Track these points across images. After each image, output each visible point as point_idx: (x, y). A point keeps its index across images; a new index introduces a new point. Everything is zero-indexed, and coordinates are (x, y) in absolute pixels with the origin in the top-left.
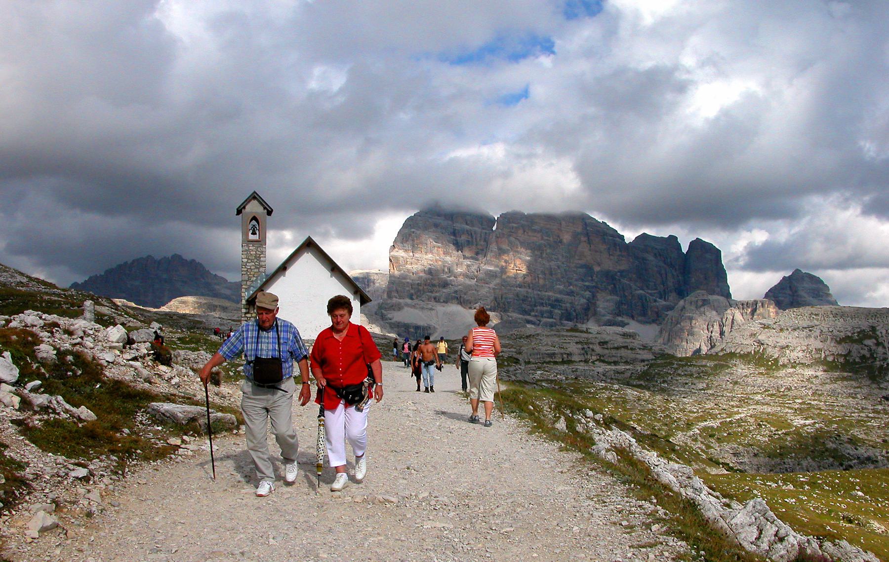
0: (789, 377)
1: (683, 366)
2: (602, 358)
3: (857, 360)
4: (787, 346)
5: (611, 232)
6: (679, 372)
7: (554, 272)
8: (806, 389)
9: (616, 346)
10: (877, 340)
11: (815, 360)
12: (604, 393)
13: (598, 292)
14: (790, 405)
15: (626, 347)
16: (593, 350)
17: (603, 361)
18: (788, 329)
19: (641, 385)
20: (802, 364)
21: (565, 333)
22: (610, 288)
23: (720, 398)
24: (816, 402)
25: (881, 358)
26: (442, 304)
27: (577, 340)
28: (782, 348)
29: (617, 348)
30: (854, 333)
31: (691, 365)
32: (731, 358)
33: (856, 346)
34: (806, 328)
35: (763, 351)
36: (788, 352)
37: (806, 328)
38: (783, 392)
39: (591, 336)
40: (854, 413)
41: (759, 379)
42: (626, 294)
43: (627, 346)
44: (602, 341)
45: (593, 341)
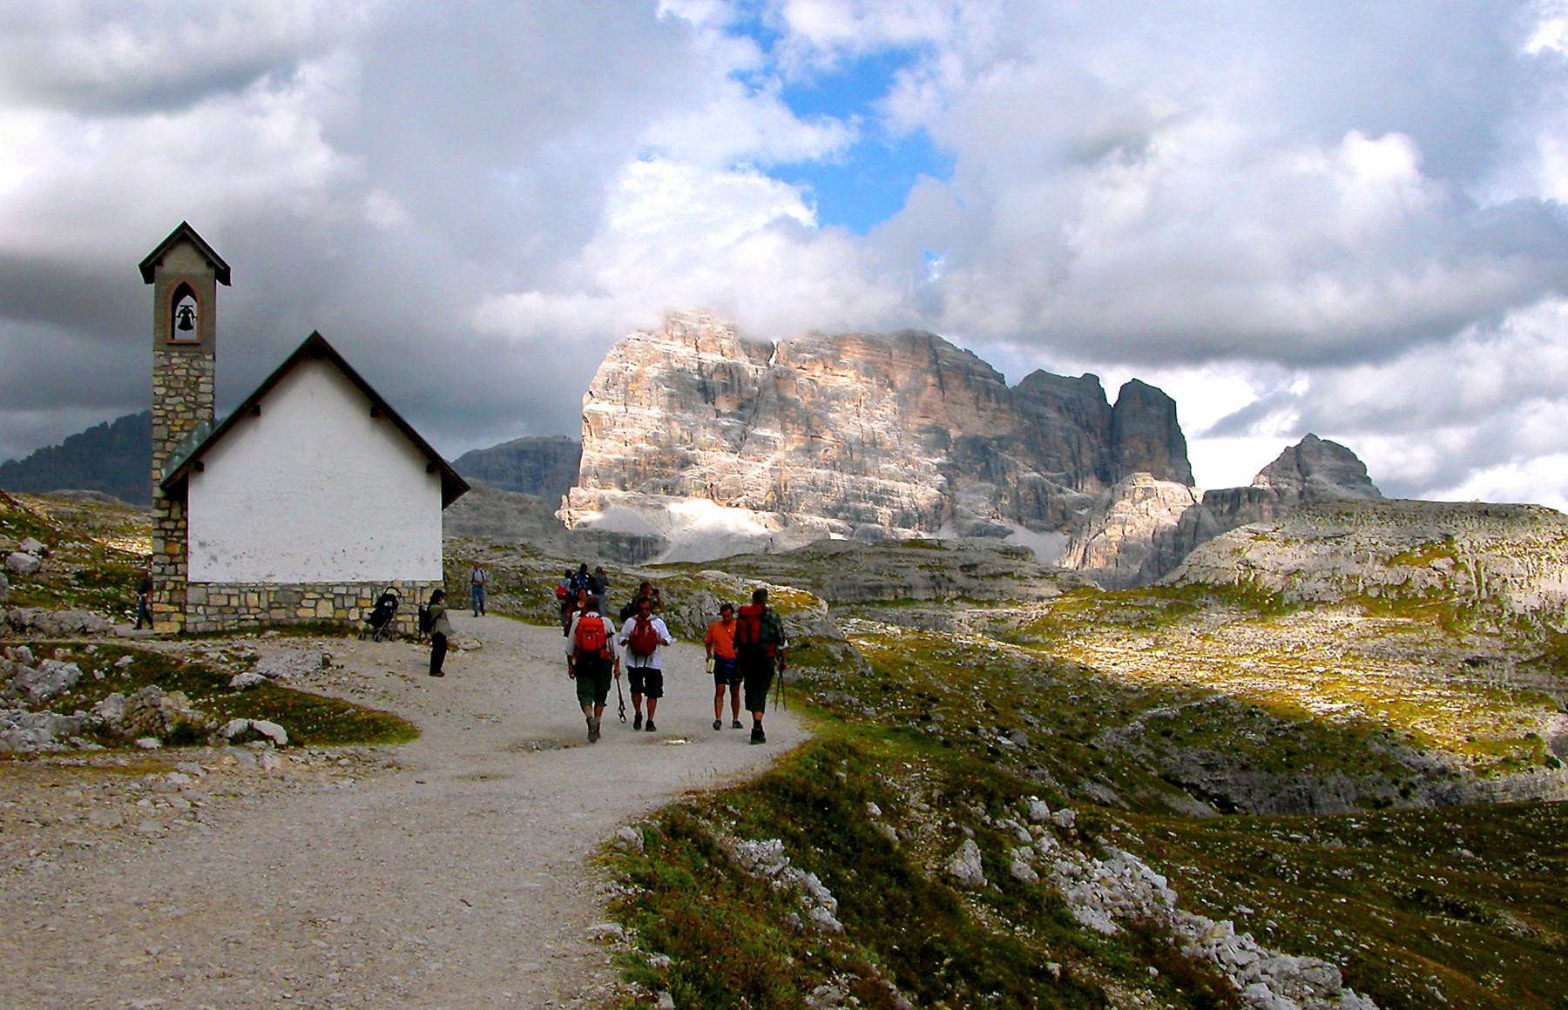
8: (1331, 648)
9: (992, 572)
32: (1198, 594)
38: (1291, 653)
39: (946, 554)
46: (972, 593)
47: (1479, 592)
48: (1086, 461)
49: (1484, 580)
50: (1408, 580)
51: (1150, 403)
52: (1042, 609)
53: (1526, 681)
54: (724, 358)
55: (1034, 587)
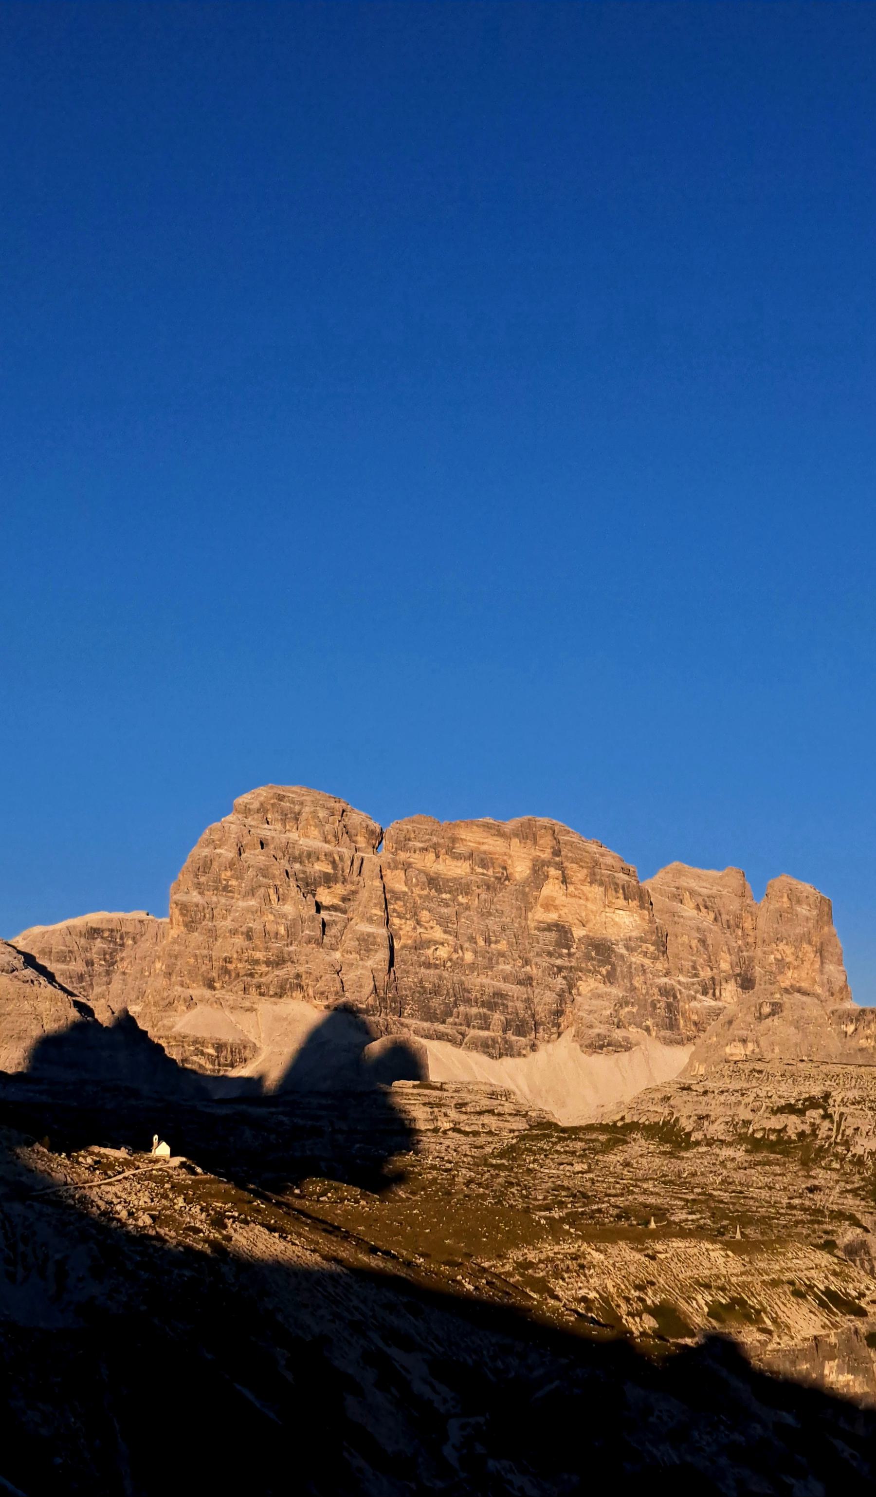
0: (699, 1158)
1: (565, 1139)
2: (457, 1126)
3: (794, 1137)
4: (708, 1116)
5: (235, 1093)
6: (558, 1148)
7: (493, 939)
8: (715, 1175)
9: (478, 1109)
10: (825, 1110)
11: (739, 1135)
12: (429, 1173)
13: (580, 979)
14: (684, 1196)
15: (491, 1112)
16: (446, 1115)
17: (459, 1131)
18: (713, 1092)
19: (503, 1164)
20: (721, 1141)
21: (410, 1091)
22: (604, 972)
23: (598, 1184)
24: (719, 1192)
25: (824, 1136)
26: (273, 999)
27: (427, 1100)
28: (701, 1118)
29: (480, 1113)
30: (800, 1100)
31: (575, 1139)
32: (632, 1131)
33: (793, 1118)
34: (737, 1091)
35: (674, 1121)
36: (706, 1123)
37: (737, 1091)
38: (685, 1178)
39: (445, 1094)
40: (762, 1207)
41: (657, 1160)
42: (637, 985)
43: (493, 1110)
44: (460, 1101)
45: (447, 1102)
46: (461, 1125)
47: (836, 1137)
48: (725, 966)
49: (842, 1128)
50: (786, 1126)
51: (799, 902)
52: (512, 1138)
53: (843, 1204)
54: (327, 846)
55: (508, 1121)
